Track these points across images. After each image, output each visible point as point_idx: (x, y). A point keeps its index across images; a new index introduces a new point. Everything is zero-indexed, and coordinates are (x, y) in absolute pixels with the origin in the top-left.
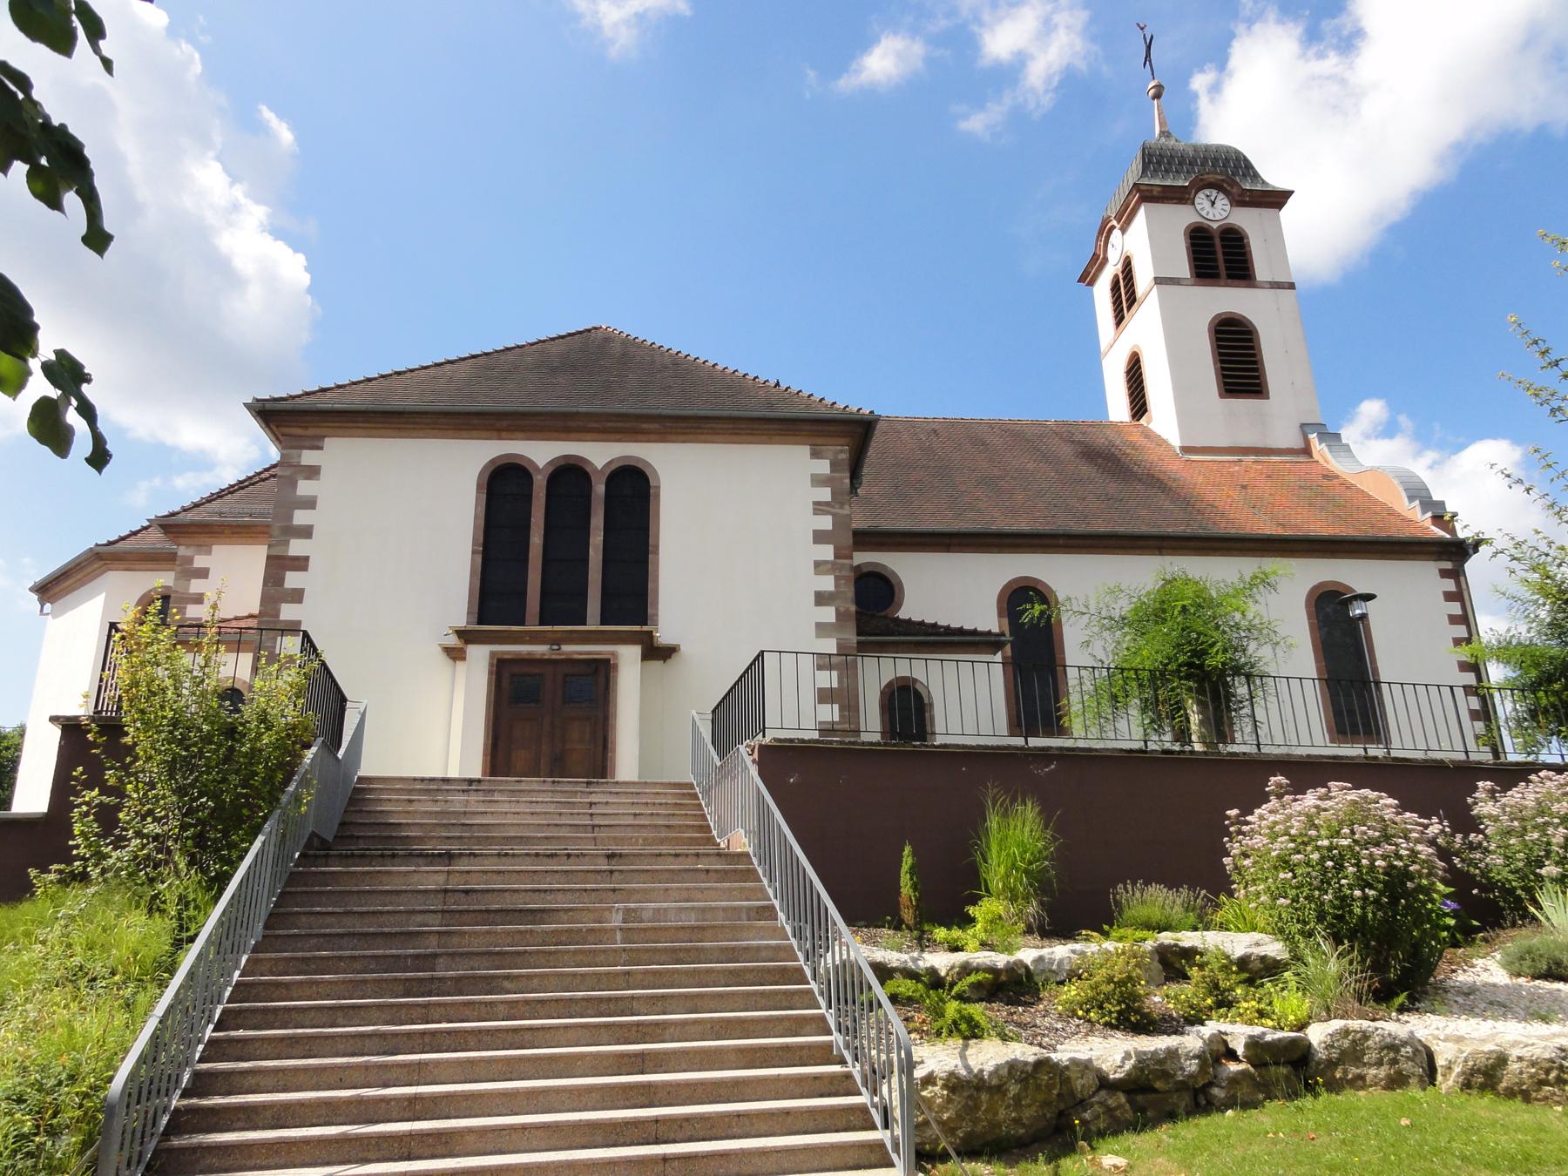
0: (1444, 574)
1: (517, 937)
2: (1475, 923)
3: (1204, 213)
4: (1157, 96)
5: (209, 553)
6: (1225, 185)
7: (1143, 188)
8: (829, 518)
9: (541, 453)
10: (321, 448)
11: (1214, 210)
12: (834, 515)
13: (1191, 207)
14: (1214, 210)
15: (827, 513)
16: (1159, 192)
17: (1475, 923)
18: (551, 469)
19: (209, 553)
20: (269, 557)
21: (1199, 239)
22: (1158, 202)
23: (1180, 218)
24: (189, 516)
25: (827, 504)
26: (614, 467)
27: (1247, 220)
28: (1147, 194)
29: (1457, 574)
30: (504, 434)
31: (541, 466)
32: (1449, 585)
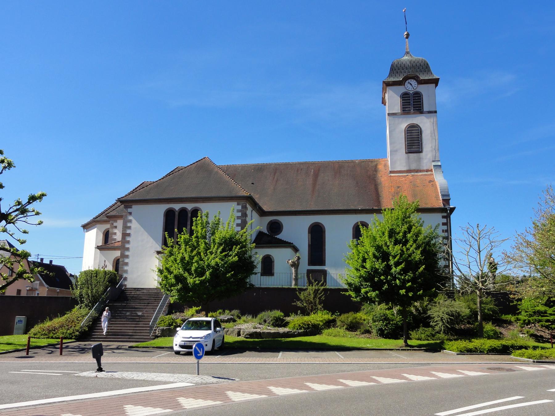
0: (443, 217)
1: (143, 324)
2: (258, 347)
3: (408, 88)
4: (407, 38)
5: (117, 222)
6: (416, 78)
7: (386, 82)
8: (240, 220)
9: (177, 207)
10: (132, 208)
11: (411, 86)
12: (241, 219)
13: (404, 86)
14: (411, 86)
15: (240, 219)
16: (392, 83)
17: (258, 347)
18: (179, 211)
19: (117, 222)
20: (122, 233)
21: (405, 97)
22: (392, 86)
23: (401, 89)
24: (123, 199)
25: (240, 217)
26: (193, 209)
27: (423, 89)
28: (388, 84)
29: (448, 217)
30: (169, 203)
31: (177, 210)
32: (445, 220)
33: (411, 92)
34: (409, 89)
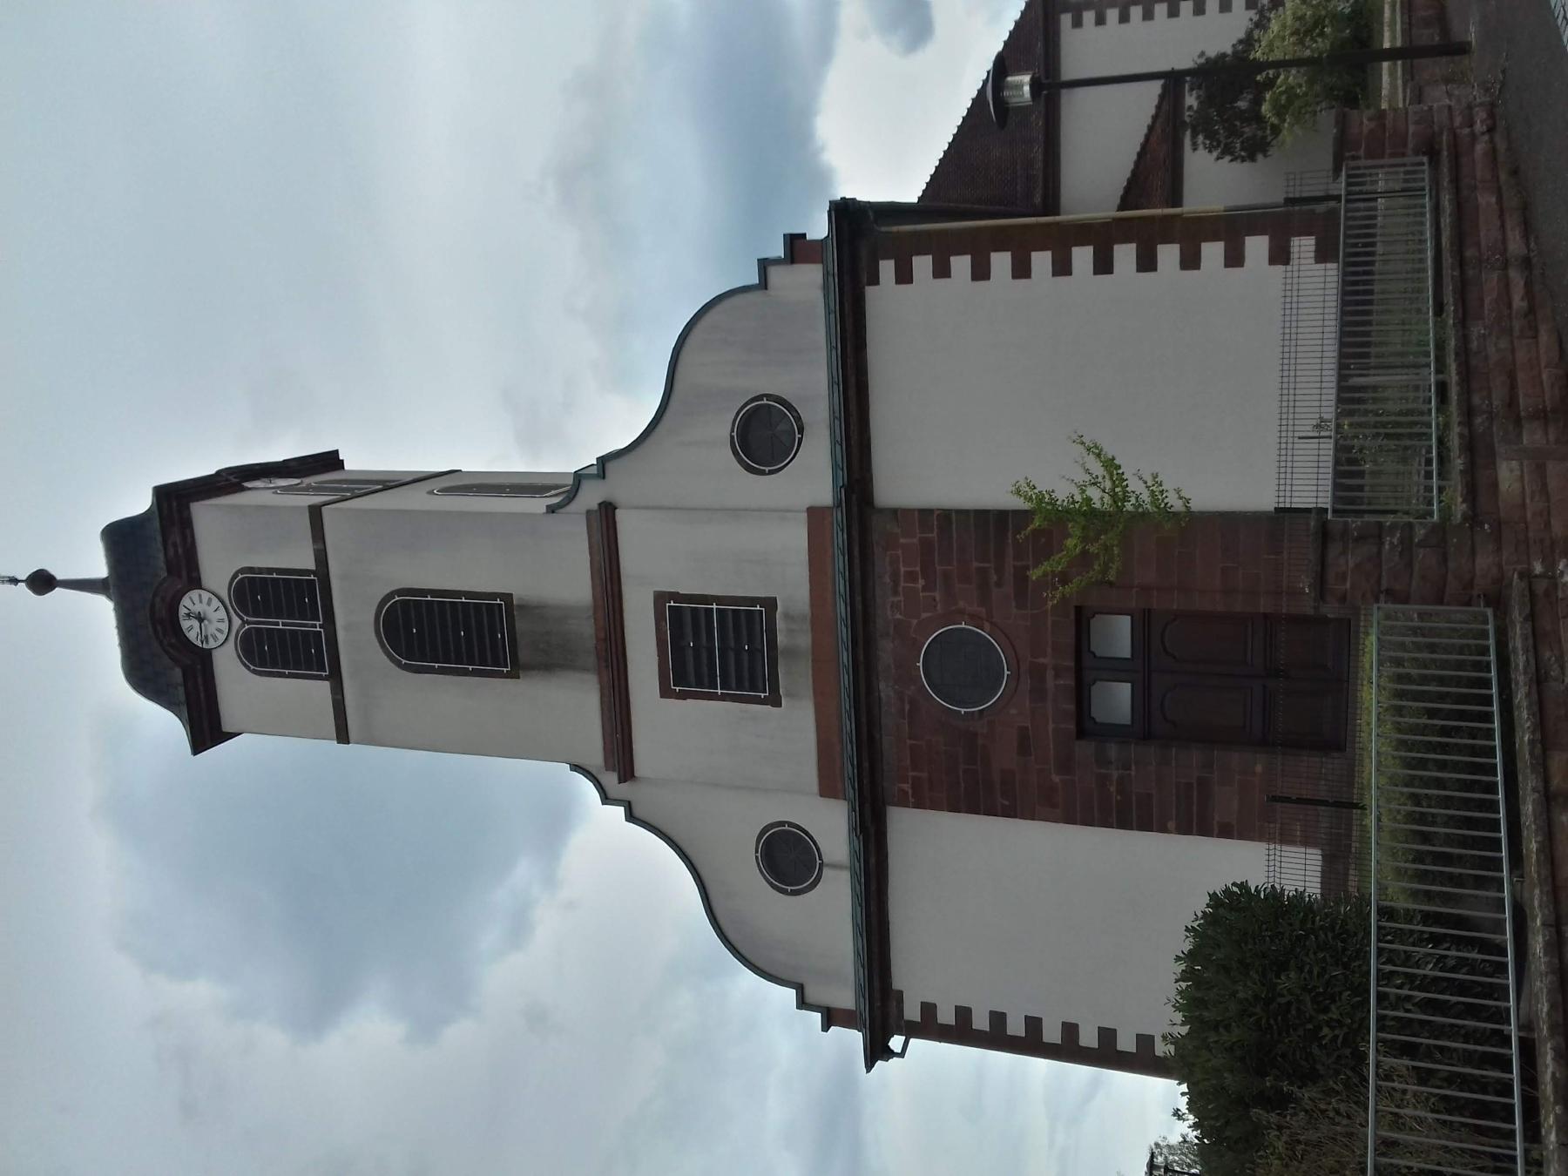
33: (237, 622)
34: (221, 621)
